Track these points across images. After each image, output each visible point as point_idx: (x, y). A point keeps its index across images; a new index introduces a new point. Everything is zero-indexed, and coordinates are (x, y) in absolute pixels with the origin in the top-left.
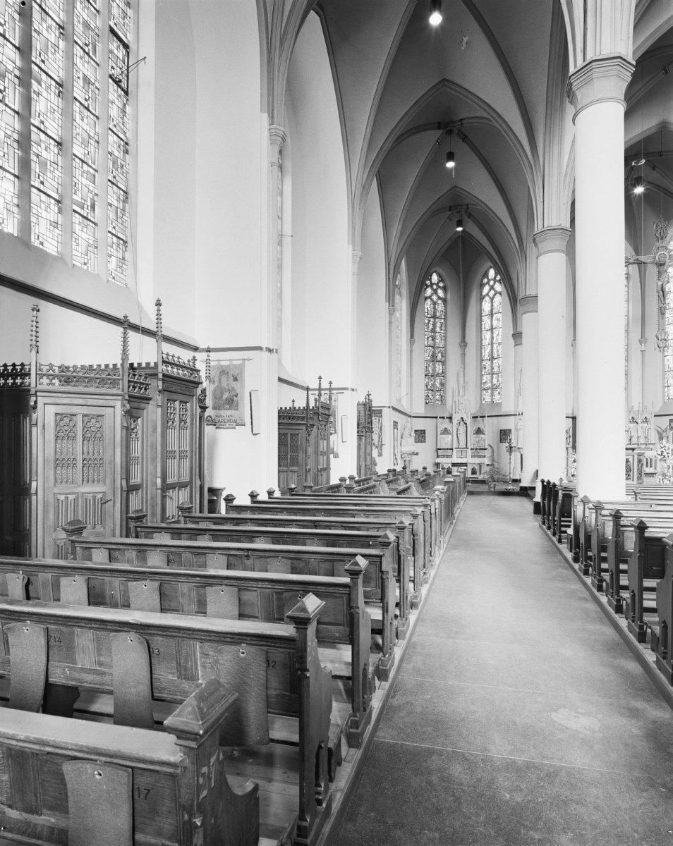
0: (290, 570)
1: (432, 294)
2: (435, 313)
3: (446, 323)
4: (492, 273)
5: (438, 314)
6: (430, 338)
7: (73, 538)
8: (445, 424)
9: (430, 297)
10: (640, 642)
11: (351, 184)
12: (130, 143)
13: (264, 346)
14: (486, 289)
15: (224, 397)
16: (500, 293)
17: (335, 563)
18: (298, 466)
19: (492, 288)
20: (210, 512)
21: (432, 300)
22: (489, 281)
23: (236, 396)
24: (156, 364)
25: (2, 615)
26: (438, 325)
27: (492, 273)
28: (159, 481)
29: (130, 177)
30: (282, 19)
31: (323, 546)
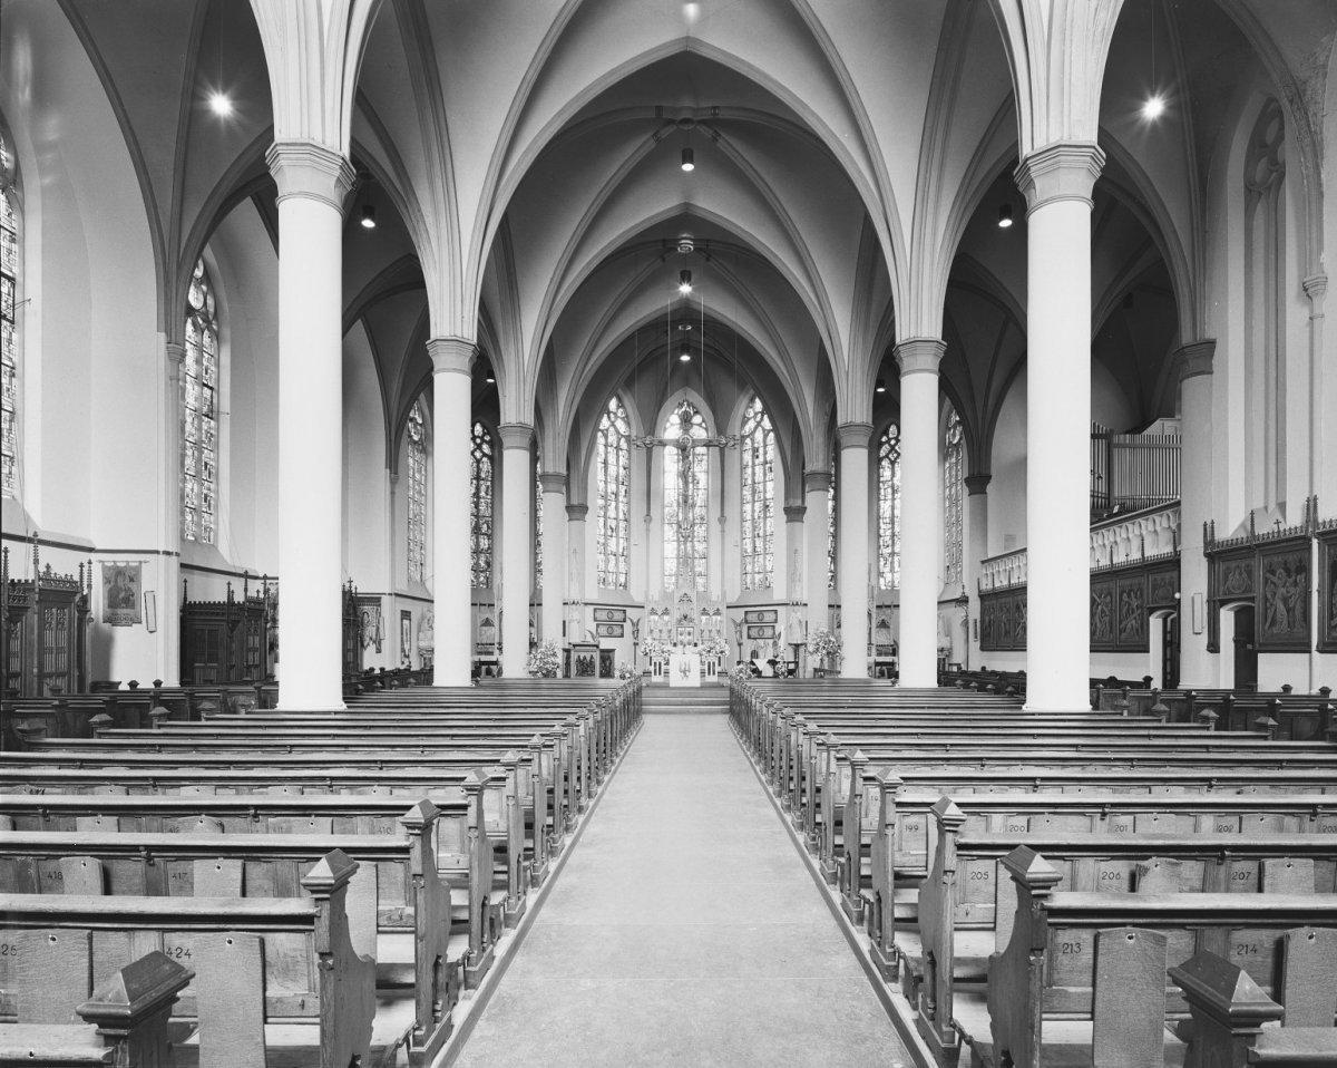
3: (492, 486)
5: (483, 475)
12: (17, 367)
13: (161, 549)
15: (121, 597)
17: (1268, 863)
18: (216, 661)
22: (890, 439)
23: (133, 595)
24: (33, 581)
25: (3, 1018)
26: (483, 488)
28: (35, 670)
29: (17, 398)
30: (180, 236)
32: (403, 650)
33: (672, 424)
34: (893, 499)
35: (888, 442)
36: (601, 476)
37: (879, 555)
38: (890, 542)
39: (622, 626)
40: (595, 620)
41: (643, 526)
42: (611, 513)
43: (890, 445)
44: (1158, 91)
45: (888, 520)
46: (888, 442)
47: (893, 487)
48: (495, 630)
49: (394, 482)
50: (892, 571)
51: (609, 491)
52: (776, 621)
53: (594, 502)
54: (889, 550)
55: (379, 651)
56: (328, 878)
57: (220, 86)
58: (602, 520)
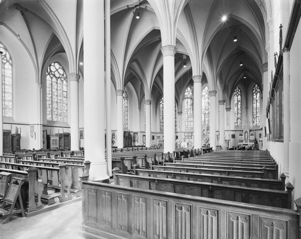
0: (241, 201)
4: (256, 86)
7: (71, 156)
8: (241, 133)
9: (162, 103)
11: (214, 73)
14: (254, 91)
16: (259, 92)
19: (256, 90)
21: (255, 93)
22: (255, 88)
27: (256, 86)
31: (171, 178)
32: (143, 142)
33: (204, 92)
34: (256, 103)
35: (255, 89)
36: (186, 105)
37: (253, 117)
38: (256, 114)
41: (245, 110)
42: (189, 113)
43: (256, 90)
44: (223, 15)
45: (255, 109)
46: (255, 89)
47: (256, 100)
49: (140, 112)
50: (256, 121)
51: (188, 108)
52: (192, 135)
53: (184, 111)
54: (256, 116)
55: (138, 142)
57: (223, 15)
58: (186, 114)
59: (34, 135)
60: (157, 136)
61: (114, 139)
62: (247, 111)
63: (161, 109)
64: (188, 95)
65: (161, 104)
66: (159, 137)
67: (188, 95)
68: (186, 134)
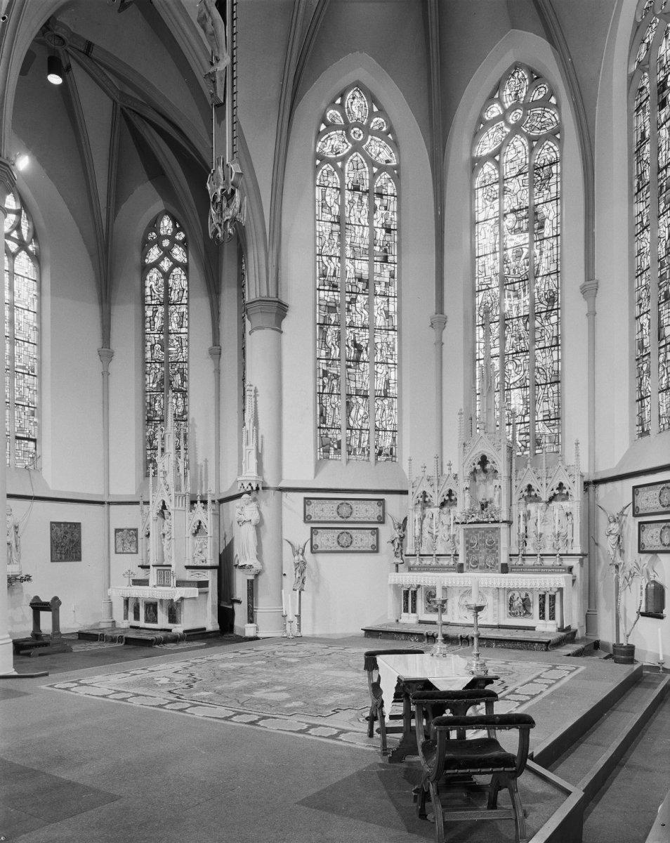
1: (161, 259)
2: (167, 293)
5: (174, 297)
6: (158, 346)
9: (156, 264)
10: (431, 690)
20: (147, 620)
21: (160, 270)
26: (175, 317)
39: (375, 532)
40: (307, 519)
41: (208, 365)
48: (86, 517)
52: (382, 520)
56: (7, 639)
59: (476, 711)
60: (116, 524)
61: (439, 646)
62: (106, 374)
63: (149, 313)
64: (344, 159)
65: (154, 274)
66: (129, 538)
67: (344, 159)
68: (325, 511)
